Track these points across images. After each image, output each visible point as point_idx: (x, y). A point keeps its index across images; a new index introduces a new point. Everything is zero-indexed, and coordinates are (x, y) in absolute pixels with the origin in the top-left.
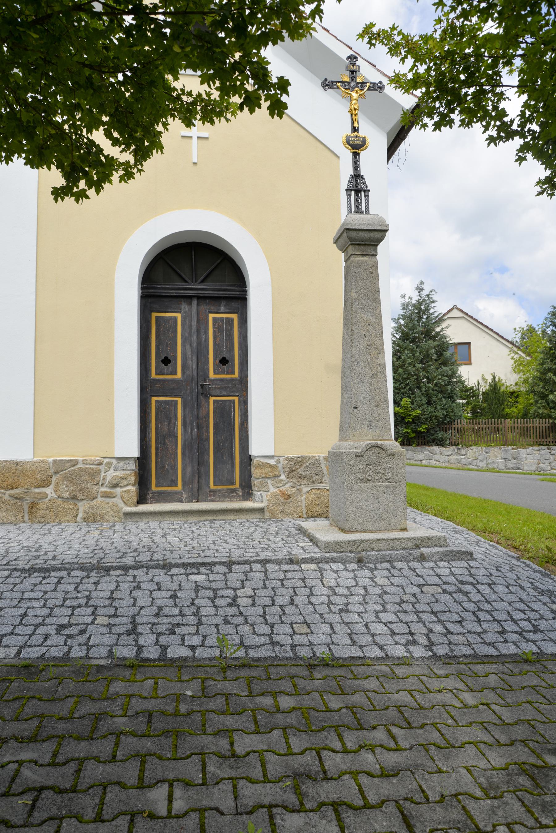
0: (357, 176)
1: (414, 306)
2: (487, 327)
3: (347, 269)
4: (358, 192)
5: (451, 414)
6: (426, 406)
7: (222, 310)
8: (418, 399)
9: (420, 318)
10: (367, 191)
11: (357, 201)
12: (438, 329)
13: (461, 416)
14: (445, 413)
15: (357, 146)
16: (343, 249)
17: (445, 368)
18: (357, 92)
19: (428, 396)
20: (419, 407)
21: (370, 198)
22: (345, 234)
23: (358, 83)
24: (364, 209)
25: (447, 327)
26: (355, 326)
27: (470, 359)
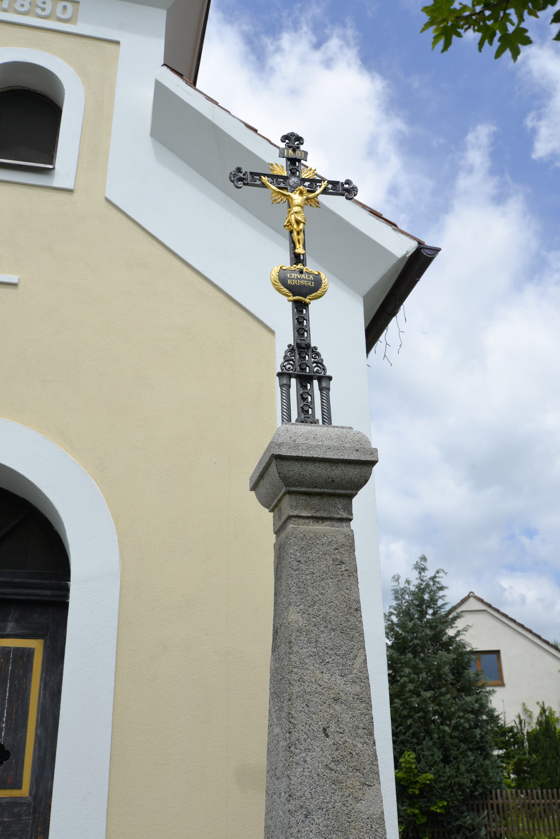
0: (302, 348)
1: (413, 594)
2: (522, 626)
3: (280, 551)
4: (305, 380)
5: (485, 780)
6: (442, 765)
7: (8, 631)
8: (427, 753)
9: (423, 614)
10: (325, 380)
11: (302, 398)
12: (451, 632)
13: (500, 783)
14: (474, 777)
15: (301, 294)
16: (272, 503)
17: (468, 699)
18: (301, 193)
19: (442, 746)
20: (431, 766)
21: (332, 394)
22: (273, 469)
23: (304, 180)
24: (318, 415)
25: (465, 630)
26: (299, 705)
27: (501, 678)
